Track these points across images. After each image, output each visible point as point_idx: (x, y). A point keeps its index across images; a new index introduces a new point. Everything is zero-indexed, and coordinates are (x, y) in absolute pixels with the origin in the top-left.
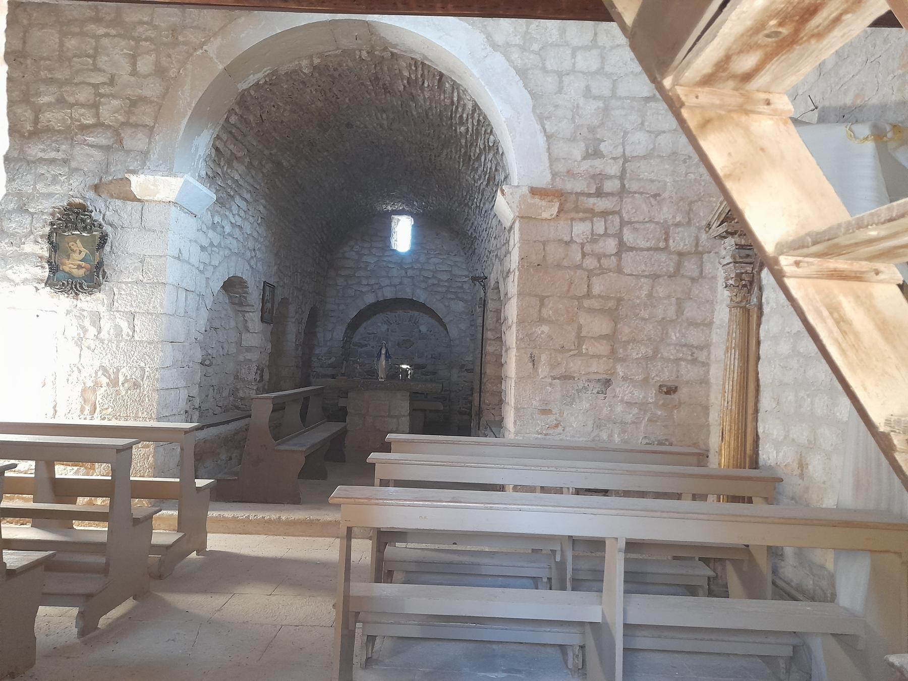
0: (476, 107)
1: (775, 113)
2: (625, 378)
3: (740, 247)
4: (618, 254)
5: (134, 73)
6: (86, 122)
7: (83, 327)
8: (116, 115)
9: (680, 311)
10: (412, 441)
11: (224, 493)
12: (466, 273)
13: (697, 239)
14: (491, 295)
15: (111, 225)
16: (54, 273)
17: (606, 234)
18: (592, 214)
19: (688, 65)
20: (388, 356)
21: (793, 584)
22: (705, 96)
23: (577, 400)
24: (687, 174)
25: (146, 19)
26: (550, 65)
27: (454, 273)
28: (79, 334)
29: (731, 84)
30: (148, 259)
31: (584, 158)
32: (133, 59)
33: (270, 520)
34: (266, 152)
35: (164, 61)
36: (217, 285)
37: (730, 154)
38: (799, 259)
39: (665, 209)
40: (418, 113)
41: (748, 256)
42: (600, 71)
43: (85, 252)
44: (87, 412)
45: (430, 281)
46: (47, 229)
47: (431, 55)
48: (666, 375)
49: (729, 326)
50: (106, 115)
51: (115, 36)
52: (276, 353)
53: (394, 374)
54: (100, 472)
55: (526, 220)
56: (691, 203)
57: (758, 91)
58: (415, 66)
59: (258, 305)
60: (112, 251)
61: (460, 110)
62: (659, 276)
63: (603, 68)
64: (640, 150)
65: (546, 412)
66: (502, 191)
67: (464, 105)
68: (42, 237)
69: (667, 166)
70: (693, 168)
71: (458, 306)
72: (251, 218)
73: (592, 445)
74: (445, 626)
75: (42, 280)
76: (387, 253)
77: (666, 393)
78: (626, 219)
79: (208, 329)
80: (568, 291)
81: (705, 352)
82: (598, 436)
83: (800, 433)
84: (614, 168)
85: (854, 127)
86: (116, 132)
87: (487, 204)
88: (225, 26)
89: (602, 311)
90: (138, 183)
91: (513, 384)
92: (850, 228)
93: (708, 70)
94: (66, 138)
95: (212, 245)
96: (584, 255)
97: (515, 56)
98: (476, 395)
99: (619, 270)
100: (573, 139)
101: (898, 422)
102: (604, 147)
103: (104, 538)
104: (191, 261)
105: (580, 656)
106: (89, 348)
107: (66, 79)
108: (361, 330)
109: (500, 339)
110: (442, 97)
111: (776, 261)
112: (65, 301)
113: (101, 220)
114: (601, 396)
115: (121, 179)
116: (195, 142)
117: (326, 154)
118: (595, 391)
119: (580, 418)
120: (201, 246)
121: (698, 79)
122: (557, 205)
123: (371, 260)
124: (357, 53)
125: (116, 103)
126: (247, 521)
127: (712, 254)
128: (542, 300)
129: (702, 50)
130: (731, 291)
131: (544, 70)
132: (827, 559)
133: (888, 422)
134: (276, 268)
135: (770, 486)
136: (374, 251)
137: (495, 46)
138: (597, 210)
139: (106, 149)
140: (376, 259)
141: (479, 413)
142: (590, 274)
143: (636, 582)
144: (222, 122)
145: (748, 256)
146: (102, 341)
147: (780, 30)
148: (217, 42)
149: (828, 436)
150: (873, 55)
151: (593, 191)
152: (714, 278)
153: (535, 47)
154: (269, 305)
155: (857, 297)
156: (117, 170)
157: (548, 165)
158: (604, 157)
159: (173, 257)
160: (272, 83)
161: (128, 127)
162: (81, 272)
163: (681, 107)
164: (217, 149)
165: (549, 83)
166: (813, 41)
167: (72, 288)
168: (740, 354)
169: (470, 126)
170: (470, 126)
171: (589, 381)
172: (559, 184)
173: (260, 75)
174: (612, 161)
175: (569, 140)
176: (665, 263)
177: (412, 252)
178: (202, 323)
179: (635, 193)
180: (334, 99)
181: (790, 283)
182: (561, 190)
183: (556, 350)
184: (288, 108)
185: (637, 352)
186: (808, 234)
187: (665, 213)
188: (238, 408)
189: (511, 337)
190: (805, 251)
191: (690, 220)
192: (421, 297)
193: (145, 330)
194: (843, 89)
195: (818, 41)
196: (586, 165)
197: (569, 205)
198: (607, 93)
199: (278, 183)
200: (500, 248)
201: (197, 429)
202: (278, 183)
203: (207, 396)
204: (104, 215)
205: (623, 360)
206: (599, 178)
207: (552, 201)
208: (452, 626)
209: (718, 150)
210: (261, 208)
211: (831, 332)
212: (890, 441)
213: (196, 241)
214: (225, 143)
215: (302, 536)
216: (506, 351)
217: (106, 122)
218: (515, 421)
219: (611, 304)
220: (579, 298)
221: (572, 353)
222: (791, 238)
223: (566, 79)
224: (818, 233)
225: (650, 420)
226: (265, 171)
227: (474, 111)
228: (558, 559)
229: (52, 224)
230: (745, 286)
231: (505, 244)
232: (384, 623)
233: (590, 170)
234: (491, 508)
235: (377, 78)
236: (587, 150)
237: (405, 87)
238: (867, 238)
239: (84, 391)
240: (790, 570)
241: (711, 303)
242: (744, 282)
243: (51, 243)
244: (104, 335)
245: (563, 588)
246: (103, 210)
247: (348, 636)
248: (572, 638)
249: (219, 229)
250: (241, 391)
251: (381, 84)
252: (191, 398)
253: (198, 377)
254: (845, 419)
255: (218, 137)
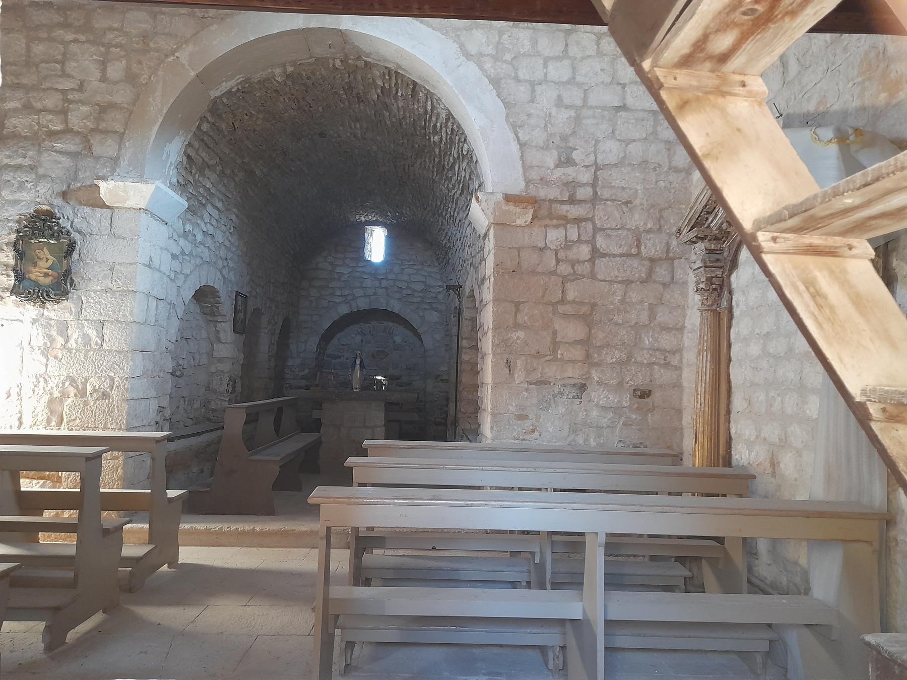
0: (450, 116)
1: (751, 95)
2: (599, 383)
3: (710, 251)
4: (592, 260)
5: (104, 79)
6: (53, 128)
7: (50, 337)
8: (85, 121)
9: (652, 315)
10: (390, 447)
11: (198, 504)
12: (440, 283)
13: (668, 244)
14: (466, 303)
15: (80, 232)
16: (20, 282)
17: (579, 241)
18: (565, 221)
19: (667, 46)
20: (362, 367)
21: (768, 582)
22: (683, 78)
23: (553, 405)
24: (657, 182)
25: (116, 25)
26: (522, 74)
27: (428, 283)
28: (45, 344)
29: (708, 65)
30: (117, 267)
31: (557, 166)
32: (103, 65)
33: (244, 531)
34: (239, 161)
35: (135, 68)
36: (188, 294)
37: (707, 134)
38: (776, 234)
39: (637, 216)
40: (392, 122)
41: (718, 260)
42: (572, 81)
43: (52, 259)
44: (53, 423)
45: (404, 292)
46: (13, 237)
47: (404, 64)
48: (641, 380)
49: (701, 330)
50: (75, 120)
51: (84, 42)
52: (249, 364)
53: (368, 384)
54: (68, 482)
55: (501, 227)
56: (661, 211)
57: (734, 73)
58: (389, 76)
59: (230, 315)
60: (80, 259)
61: (434, 119)
62: (632, 282)
63: (574, 78)
64: (612, 159)
65: (522, 417)
66: (477, 198)
67: (438, 114)
68: (7, 244)
69: (638, 174)
70: (663, 176)
71: (434, 317)
72: (223, 227)
73: (570, 448)
74: (426, 630)
75: (7, 289)
76: (361, 264)
77: (640, 397)
78: (599, 226)
79: (179, 339)
80: (543, 296)
81: (677, 356)
82: (574, 440)
83: (772, 432)
84: (586, 176)
85: (818, 131)
86: (85, 138)
87: (461, 212)
88: (197, 33)
89: (576, 316)
90: (106, 189)
91: (490, 390)
92: (826, 198)
93: (686, 51)
94: (33, 144)
95: (183, 253)
96: (558, 261)
97: (488, 66)
98: (452, 405)
99: (593, 276)
100: (546, 148)
101: (874, 391)
102: (576, 155)
103: (72, 551)
104: (162, 269)
105: (561, 658)
106: (56, 358)
107: (33, 85)
108: (335, 341)
109: (476, 348)
110: (416, 106)
111: (754, 237)
112: (31, 310)
113: (69, 227)
114: (577, 401)
115: (90, 186)
116: (167, 149)
117: (299, 163)
118: (571, 396)
119: (557, 422)
120: (172, 254)
121: (677, 60)
122: (531, 211)
123: (345, 271)
124: (331, 61)
125: (85, 109)
126: (220, 533)
127: (682, 260)
128: (517, 305)
129: (680, 29)
130: (702, 295)
131: (517, 79)
132: (800, 554)
133: (864, 392)
134: (248, 277)
135: (742, 483)
136: (347, 261)
137: (468, 56)
138: (570, 216)
139: (74, 155)
140: (350, 270)
141: (455, 423)
142: (565, 280)
143: (614, 582)
144: (194, 129)
145: (718, 260)
146: (70, 350)
147: (756, 7)
148: (190, 48)
149: (798, 434)
150: (833, 64)
151: (566, 198)
152: (685, 283)
153: (508, 57)
154: (241, 315)
155: (831, 272)
156: (85, 177)
157: (521, 172)
158: (576, 165)
159: (144, 264)
160: (245, 90)
161: (98, 133)
162: (48, 281)
163: (660, 89)
164: (189, 157)
165: (522, 93)
166: (787, 19)
167: (38, 297)
168: (712, 356)
169: (444, 135)
170: (444, 135)
171: (564, 385)
172: (533, 191)
173: (232, 83)
174: (584, 169)
175: (542, 148)
176: (638, 269)
177: (385, 262)
178: (173, 333)
179: (607, 200)
180: (307, 108)
181: (767, 258)
182: (535, 197)
183: (533, 356)
184: (261, 116)
185: (611, 357)
186: (785, 208)
187: (637, 220)
188: (209, 420)
189: (487, 344)
190: (783, 225)
191: (660, 227)
192: (396, 307)
193: (114, 338)
194: (806, 96)
195: (791, 19)
196: (559, 172)
197: (543, 212)
198: (578, 102)
199: (250, 192)
200: (475, 256)
201: (169, 439)
202: (250, 192)
203: (178, 407)
204: (72, 223)
205: (598, 365)
206: (572, 185)
207: (525, 208)
208: (433, 630)
209: (695, 128)
210: (233, 217)
211: (807, 306)
212: (866, 410)
213: (166, 249)
214: (197, 150)
215: (277, 547)
216: (482, 358)
217: (75, 128)
218: (492, 427)
219: (585, 309)
220: (554, 304)
221: (547, 358)
222: (768, 214)
223: (538, 89)
224: (794, 206)
225: (624, 424)
226: (237, 179)
227: (447, 120)
228: (537, 561)
229: (18, 231)
230: (715, 290)
231: (479, 252)
232: (362, 629)
233: (563, 177)
234: (472, 506)
235: (351, 88)
236: (560, 158)
237: (378, 96)
238: (842, 207)
239: (51, 401)
240: (765, 568)
241: (683, 308)
242: (714, 286)
243: (17, 250)
244: (72, 344)
245: (542, 586)
246: (71, 217)
247: (327, 644)
248: (551, 638)
249: (190, 237)
250: (212, 403)
251: (354, 93)
252: (161, 409)
253: (169, 387)
254: (815, 416)
255: (190, 145)
